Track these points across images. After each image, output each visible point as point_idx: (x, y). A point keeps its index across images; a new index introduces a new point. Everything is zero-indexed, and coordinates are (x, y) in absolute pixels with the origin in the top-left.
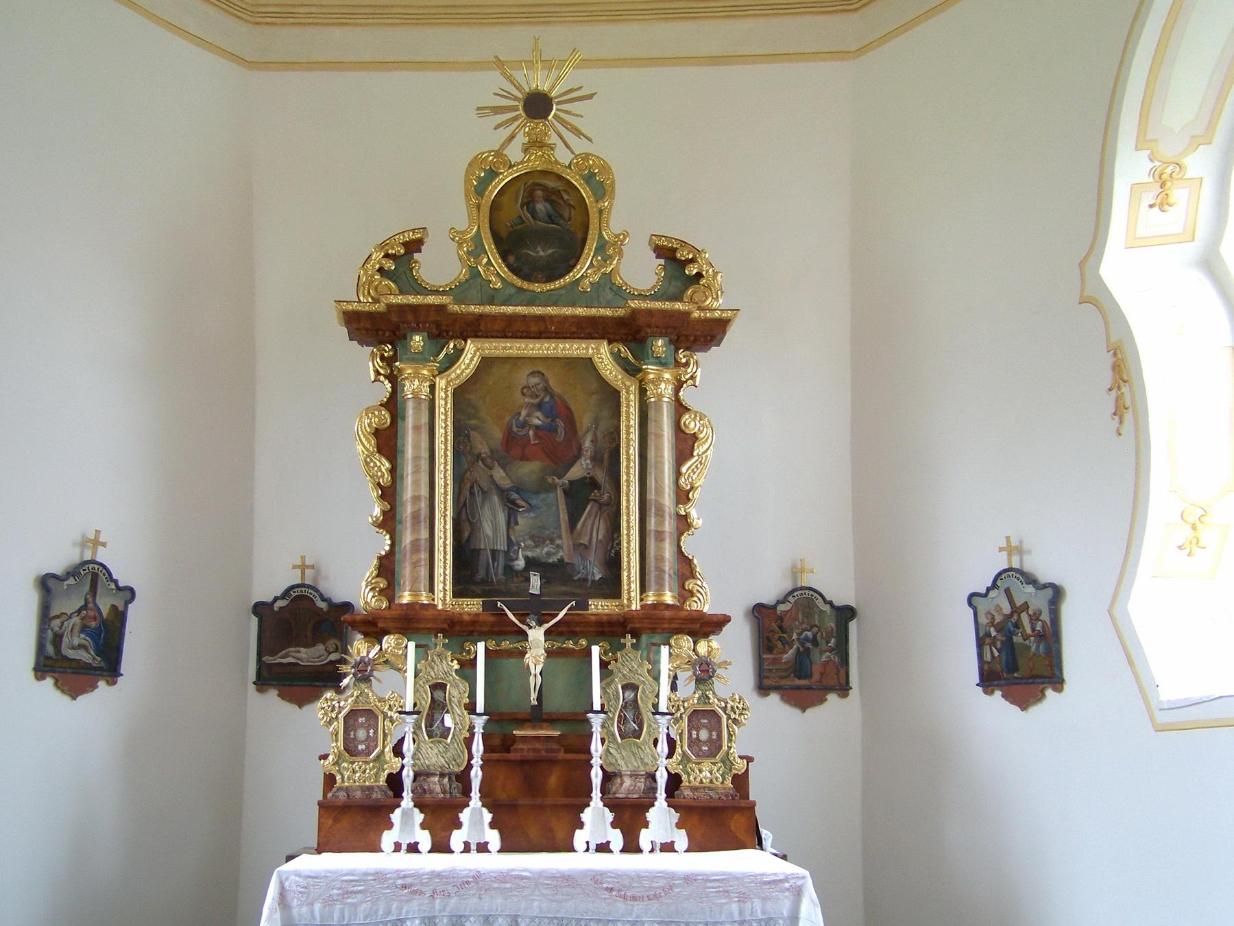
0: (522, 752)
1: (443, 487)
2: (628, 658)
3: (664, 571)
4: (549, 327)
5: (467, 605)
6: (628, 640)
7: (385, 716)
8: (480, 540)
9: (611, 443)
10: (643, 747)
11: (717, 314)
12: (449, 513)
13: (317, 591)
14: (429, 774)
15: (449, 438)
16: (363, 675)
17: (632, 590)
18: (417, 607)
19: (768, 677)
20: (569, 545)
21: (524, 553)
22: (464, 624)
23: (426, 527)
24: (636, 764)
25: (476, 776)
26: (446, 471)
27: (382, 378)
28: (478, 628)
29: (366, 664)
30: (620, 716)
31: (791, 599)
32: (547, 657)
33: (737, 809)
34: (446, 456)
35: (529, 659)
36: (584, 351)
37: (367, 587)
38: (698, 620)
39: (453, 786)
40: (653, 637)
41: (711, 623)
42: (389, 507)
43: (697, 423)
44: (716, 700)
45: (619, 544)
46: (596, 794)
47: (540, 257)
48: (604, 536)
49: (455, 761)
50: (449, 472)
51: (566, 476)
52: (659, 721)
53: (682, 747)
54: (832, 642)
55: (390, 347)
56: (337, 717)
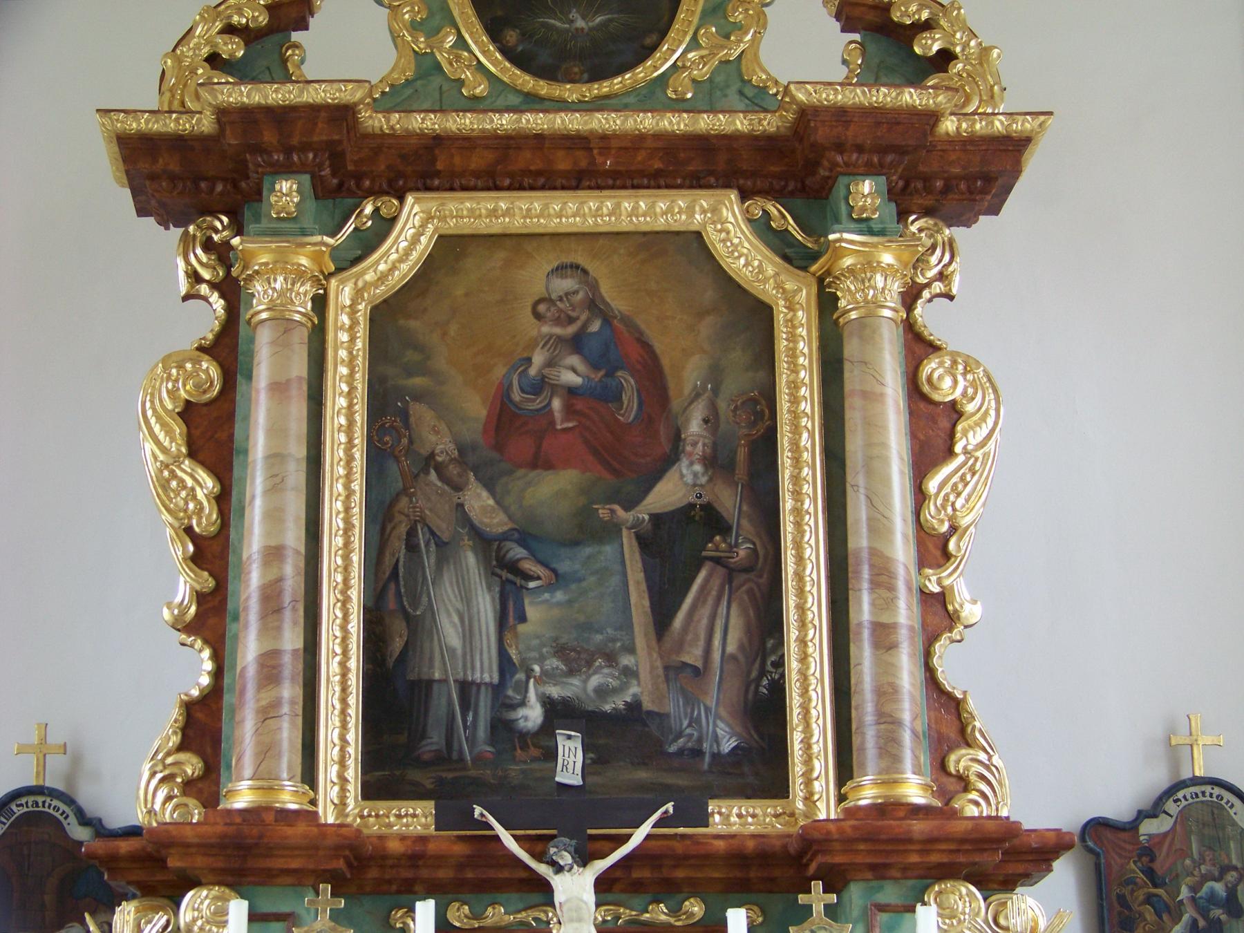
1: (341, 532)
3: (897, 723)
4: (599, 160)
5: (399, 816)
6: (817, 898)
8: (431, 659)
9: (754, 424)
11: (999, 125)
12: (356, 594)
13: (70, 801)
15: (358, 418)
17: (815, 774)
18: (269, 818)
20: (653, 668)
21: (541, 689)
22: (390, 862)
23: (295, 623)
26: (350, 493)
27: (204, 289)
28: (425, 873)
34: (350, 459)
36: (684, 217)
37: (153, 774)
38: (1000, 840)
41: (1020, 853)
42: (211, 583)
43: (960, 378)
45: (780, 664)
47: (577, 29)
48: (741, 647)
50: (357, 497)
51: (645, 502)
55: (225, 219)
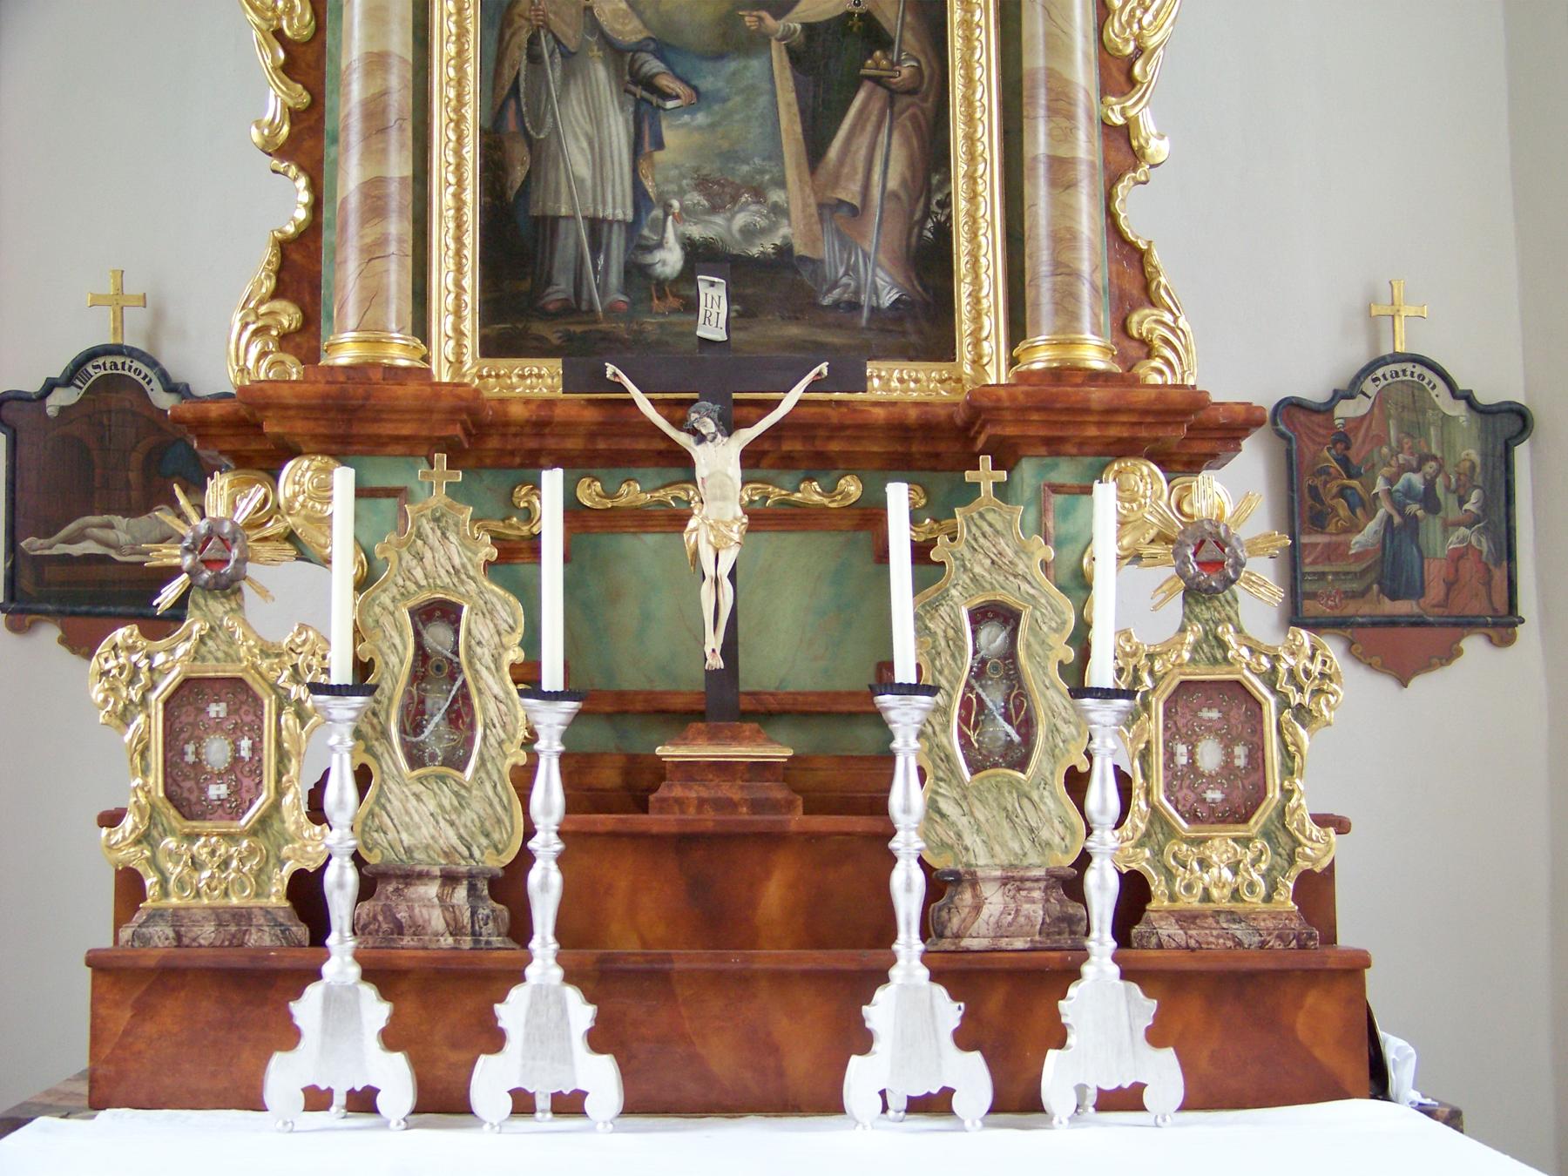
0: (682, 812)
2: (986, 528)
5: (522, 377)
6: (986, 475)
7: (283, 700)
8: (557, 192)
10: (1035, 796)
12: (471, 113)
13: (152, 363)
14: (411, 877)
16: (218, 575)
17: (984, 334)
18: (377, 375)
19: (1313, 596)
20: (805, 206)
21: (681, 228)
22: (513, 430)
23: (402, 146)
24: (1016, 846)
25: (544, 886)
28: (551, 443)
29: (226, 543)
30: (966, 704)
31: (1369, 387)
32: (748, 531)
33: (1314, 976)
35: (698, 532)
37: (245, 325)
38: (1185, 413)
39: (483, 912)
40: (1054, 467)
44: (1244, 651)
45: (946, 204)
46: (908, 944)
49: (487, 835)
52: (1093, 716)
53: (1148, 792)
54: (1473, 500)
56: (144, 699)
